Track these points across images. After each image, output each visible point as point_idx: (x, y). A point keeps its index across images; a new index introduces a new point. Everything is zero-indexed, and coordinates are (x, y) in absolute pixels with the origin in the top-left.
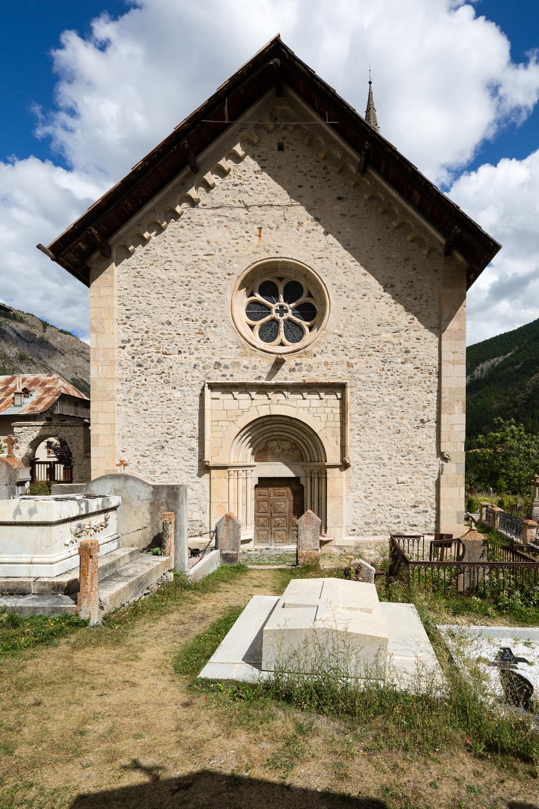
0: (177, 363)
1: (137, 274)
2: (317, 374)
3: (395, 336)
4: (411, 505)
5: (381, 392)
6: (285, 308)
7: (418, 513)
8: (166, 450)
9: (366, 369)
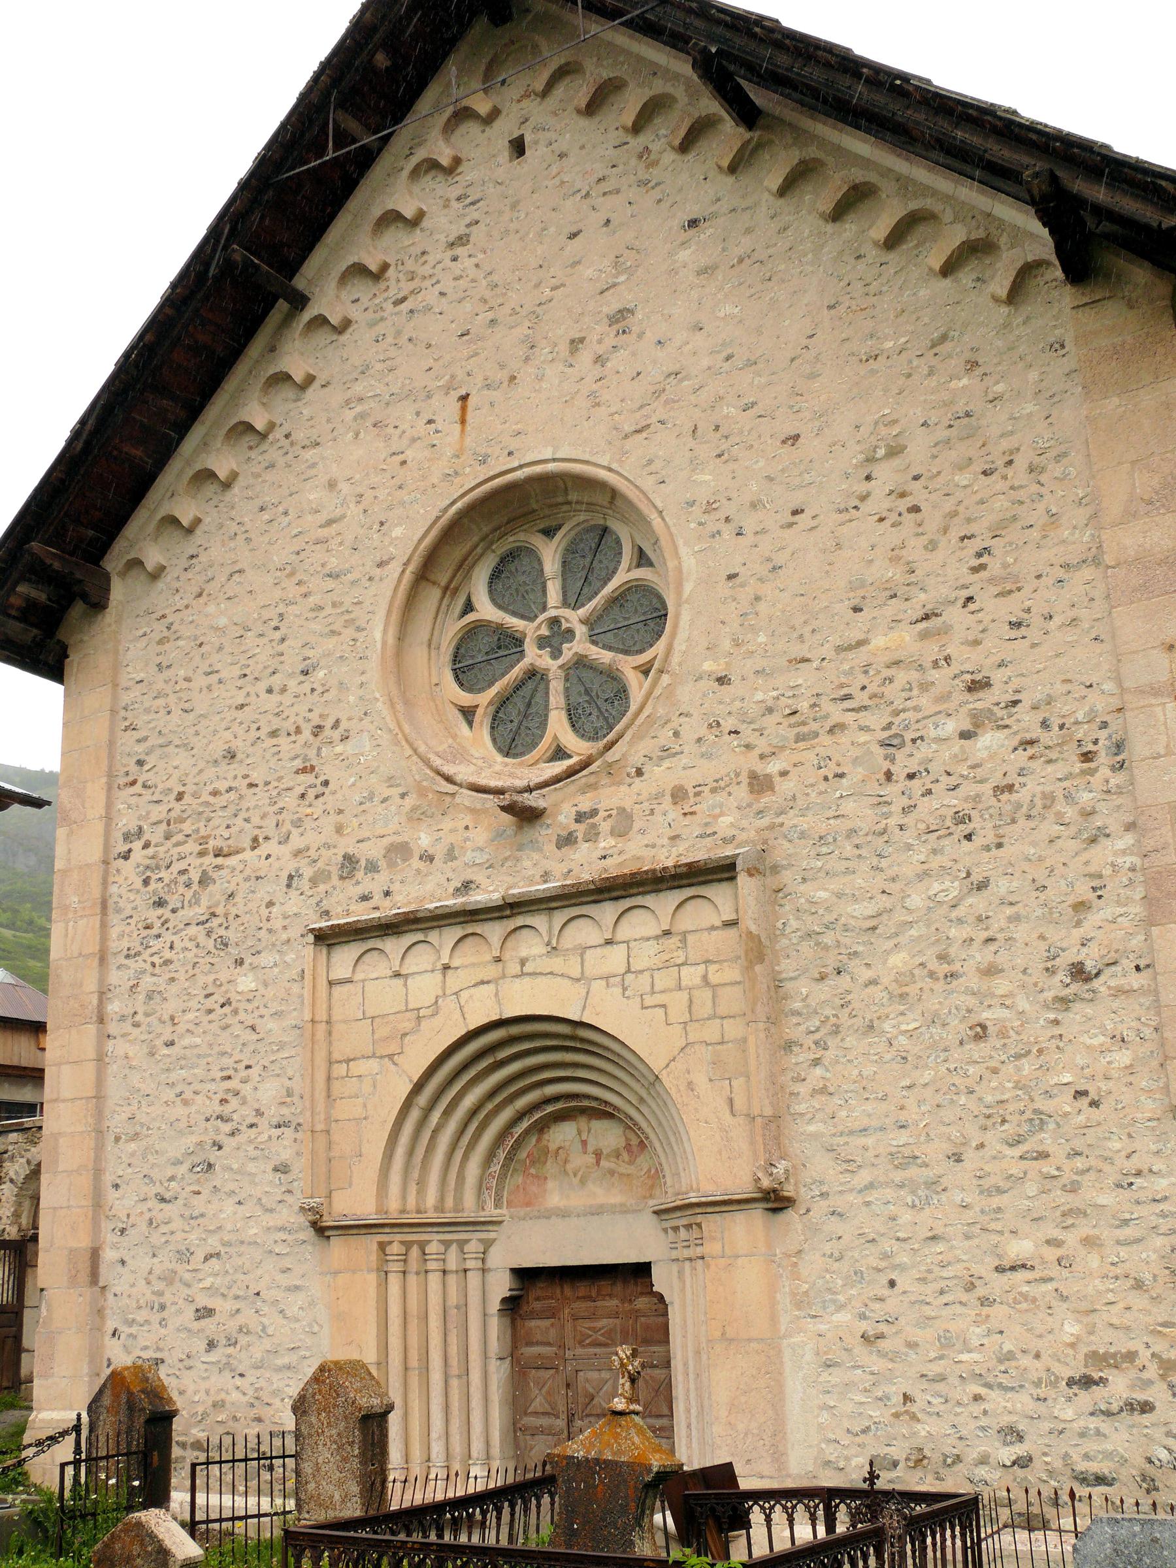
0: (247, 879)
1: (166, 633)
3: (924, 636)
4: (1067, 1373)
5: (891, 873)
6: (565, 625)
7: (1108, 1414)
8: (219, 1177)
9: (823, 786)
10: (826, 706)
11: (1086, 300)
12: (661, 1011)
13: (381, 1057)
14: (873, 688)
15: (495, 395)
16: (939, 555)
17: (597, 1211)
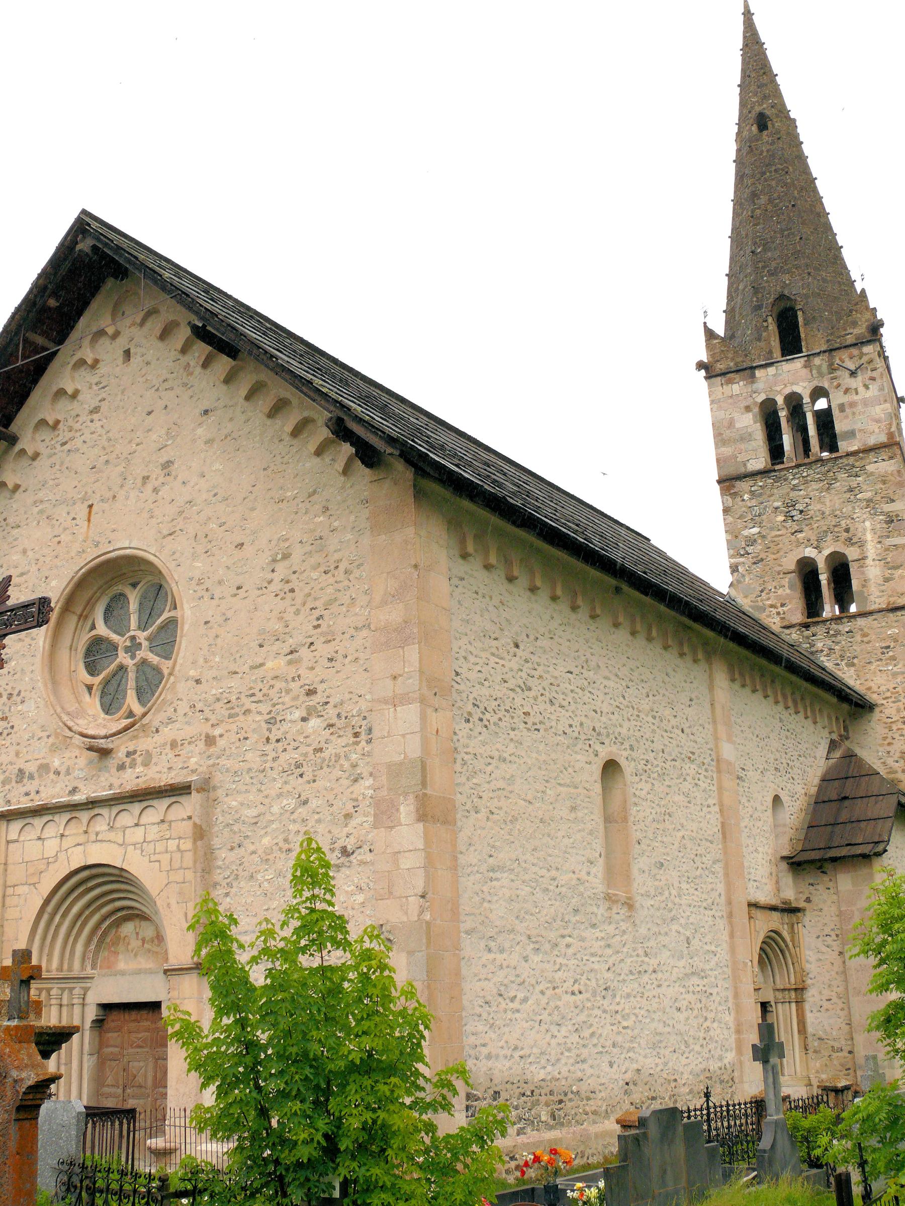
2: (158, 769)
3: (290, 663)
5: (265, 793)
6: (138, 641)
9: (238, 744)
10: (244, 699)
11: (376, 478)
12: (157, 864)
13: (30, 885)
14: (265, 691)
15: (106, 506)
16: (301, 618)
17: (139, 972)
